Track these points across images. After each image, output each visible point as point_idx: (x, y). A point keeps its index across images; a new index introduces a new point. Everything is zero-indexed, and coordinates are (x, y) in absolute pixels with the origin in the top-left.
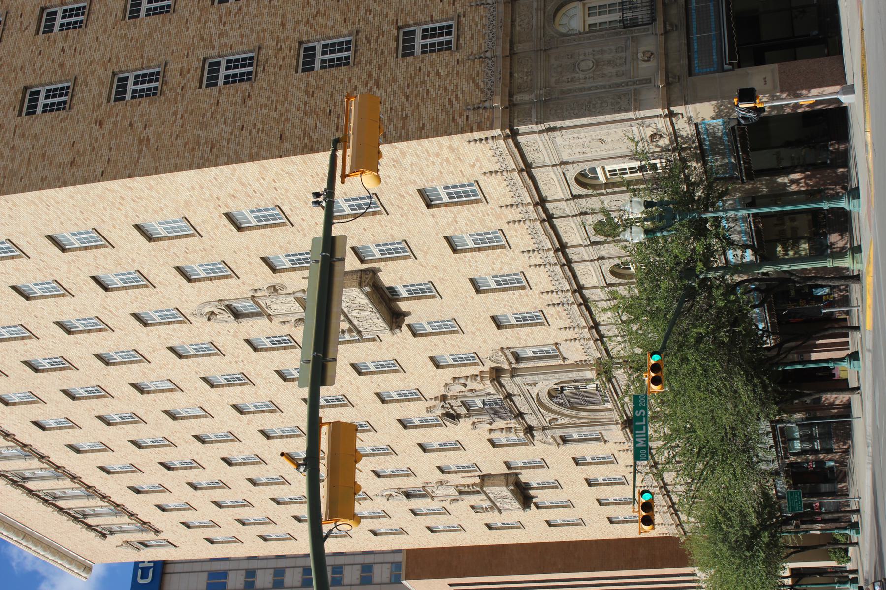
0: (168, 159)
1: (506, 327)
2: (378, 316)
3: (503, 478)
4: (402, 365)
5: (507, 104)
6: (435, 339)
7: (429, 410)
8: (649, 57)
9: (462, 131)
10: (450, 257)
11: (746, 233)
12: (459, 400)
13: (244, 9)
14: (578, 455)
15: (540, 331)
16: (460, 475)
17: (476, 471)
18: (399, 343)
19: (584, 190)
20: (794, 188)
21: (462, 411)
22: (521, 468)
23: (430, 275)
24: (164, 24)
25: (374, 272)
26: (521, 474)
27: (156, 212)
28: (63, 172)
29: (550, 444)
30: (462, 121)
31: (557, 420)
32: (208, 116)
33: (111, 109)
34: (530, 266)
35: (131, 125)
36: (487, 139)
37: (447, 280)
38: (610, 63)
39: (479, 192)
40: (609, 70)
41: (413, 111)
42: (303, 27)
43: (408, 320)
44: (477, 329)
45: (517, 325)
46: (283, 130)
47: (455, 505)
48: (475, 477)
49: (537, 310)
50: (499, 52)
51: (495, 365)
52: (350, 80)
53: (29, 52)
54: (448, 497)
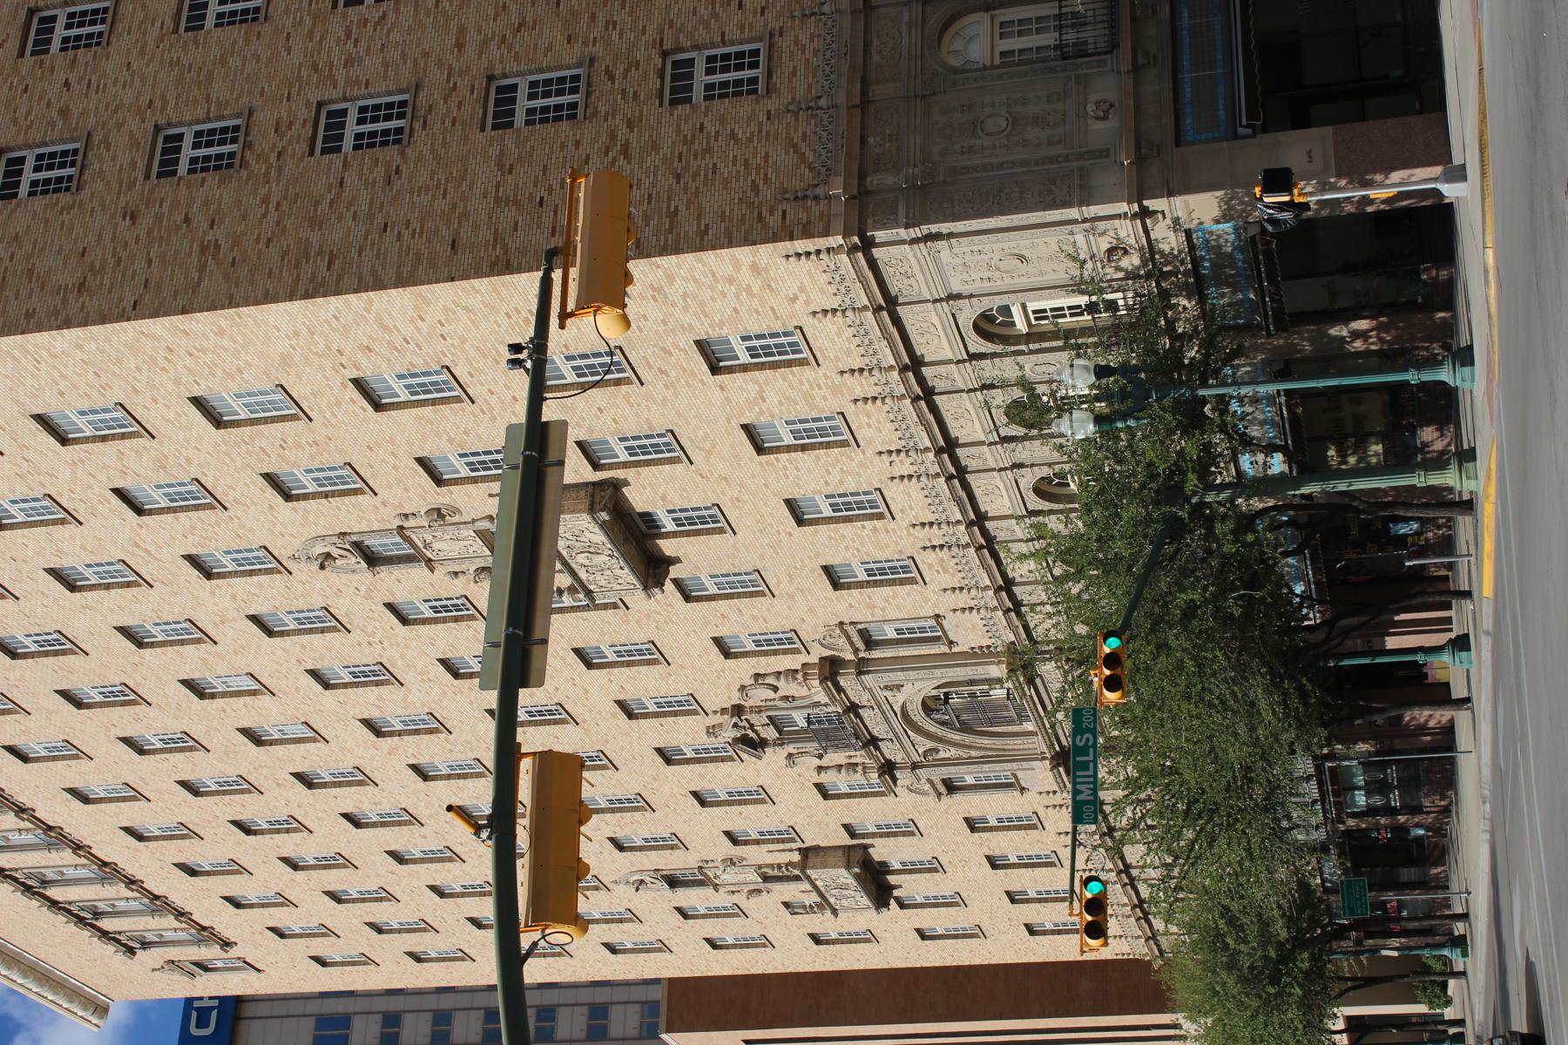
0: (252, 282)
1: (849, 586)
2: (622, 564)
3: (840, 853)
4: (664, 652)
5: (855, 191)
6: (722, 605)
7: (711, 731)
8: (1106, 112)
9: (775, 239)
10: (751, 460)
11: (1273, 424)
12: (764, 715)
13: (391, 17)
14: (974, 814)
15: (908, 594)
16: (765, 847)
17: (792, 840)
18: (658, 613)
19: (989, 344)
20: (1359, 345)
21: (770, 733)
22: (873, 835)
23: (715, 492)
24: (247, 41)
25: (616, 486)
26: (872, 846)
27: (228, 375)
28: (65, 301)
29: (924, 794)
30: (774, 221)
31: (937, 751)
32: (325, 205)
33: (151, 191)
34: (893, 478)
35: (187, 220)
36: (818, 252)
37: (745, 502)
38: (1037, 120)
39: (803, 346)
40: (1034, 134)
41: (689, 202)
42: (494, 51)
43: (675, 572)
44: (797, 589)
45: (868, 582)
46: (457, 233)
47: (754, 900)
48: (791, 850)
49: (904, 557)
50: (841, 100)
51: (828, 653)
52: (577, 144)
53: (5, 89)
54: (743, 887)
